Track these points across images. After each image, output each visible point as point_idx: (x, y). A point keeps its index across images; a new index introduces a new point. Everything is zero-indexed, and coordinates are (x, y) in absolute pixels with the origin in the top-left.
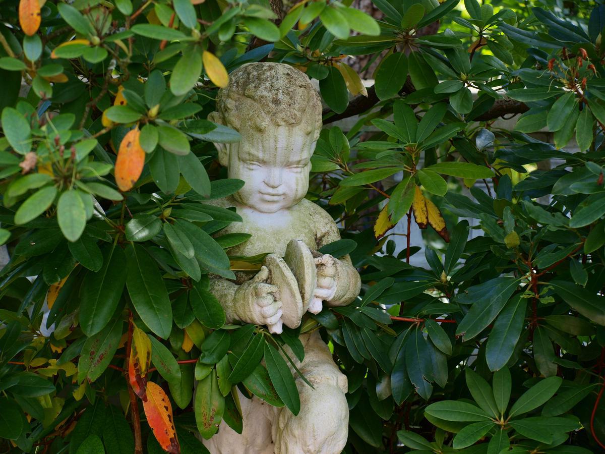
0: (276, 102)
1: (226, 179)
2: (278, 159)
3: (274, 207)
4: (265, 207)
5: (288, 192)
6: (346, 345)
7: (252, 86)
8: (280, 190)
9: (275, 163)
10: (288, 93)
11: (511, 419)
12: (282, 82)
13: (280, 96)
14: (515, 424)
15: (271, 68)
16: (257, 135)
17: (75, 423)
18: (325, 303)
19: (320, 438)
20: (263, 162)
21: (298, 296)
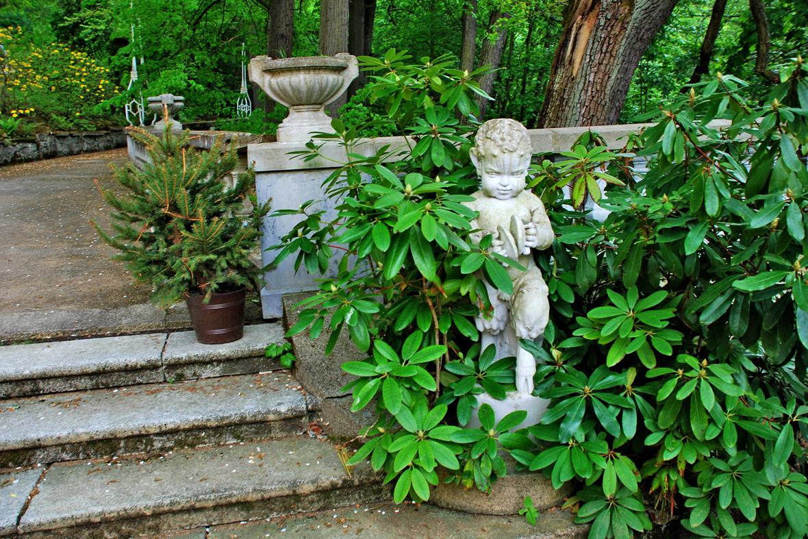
0: (503, 139)
1: (437, 240)
2: (506, 171)
3: (507, 197)
4: (501, 197)
5: (513, 188)
6: (771, 193)
7: (489, 132)
8: (508, 188)
9: (504, 173)
10: (509, 135)
11: (637, 313)
12: (507, 128)
13: (505, 137)
14: (638, 316)
15: (501, 121)
16: (494, 159)
17: (453, 89)
18: (532, 249)
19: (533, 321)
20: (498, 173)
21: (515, 246)
